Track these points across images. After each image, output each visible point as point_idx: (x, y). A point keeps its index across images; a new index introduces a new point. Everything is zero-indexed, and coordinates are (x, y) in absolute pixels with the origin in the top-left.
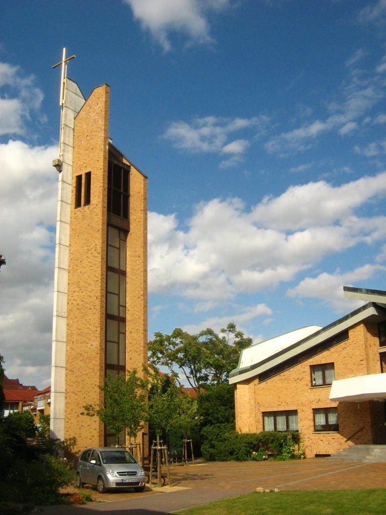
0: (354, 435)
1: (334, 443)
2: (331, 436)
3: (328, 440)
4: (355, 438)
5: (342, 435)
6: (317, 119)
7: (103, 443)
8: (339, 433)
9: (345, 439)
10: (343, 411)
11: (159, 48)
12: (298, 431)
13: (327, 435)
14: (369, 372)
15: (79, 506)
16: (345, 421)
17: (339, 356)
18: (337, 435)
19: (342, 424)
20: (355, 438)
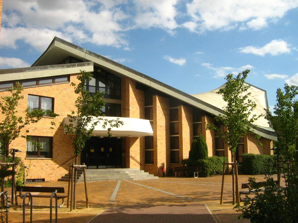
0: (66, 162)
1: (47, 168)
2: (44, 162)
3: (42, 166)
4: (67, 164)
5: (55, 162)
6: (186, 4)
7: (225, 152)
8: (52, 160)
9: (58, 166)
10: (58, 141)
11: (276, 116)
12: (21, 158)
13: (41, 160)
14: (137, 118)
15: (165, 171)
16: (59, 149)
17: (60, 93)
18: (49, 162)
19: (56, 151)
20: (67, 164)
